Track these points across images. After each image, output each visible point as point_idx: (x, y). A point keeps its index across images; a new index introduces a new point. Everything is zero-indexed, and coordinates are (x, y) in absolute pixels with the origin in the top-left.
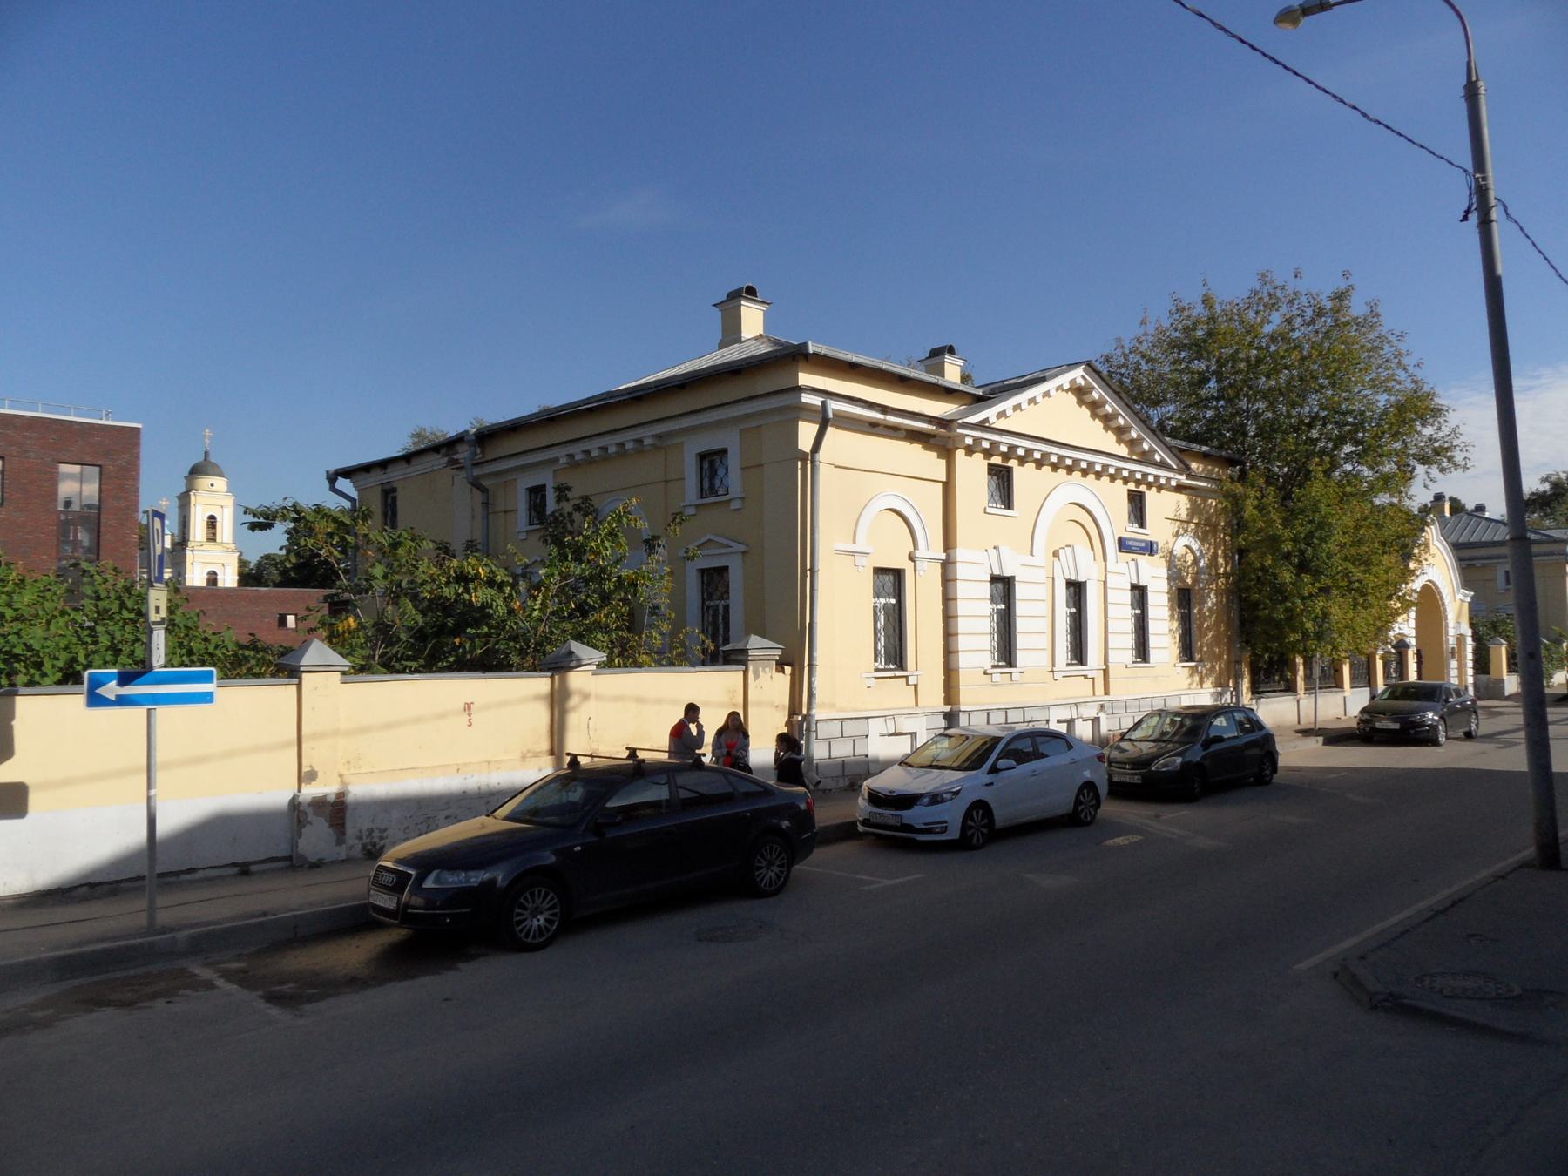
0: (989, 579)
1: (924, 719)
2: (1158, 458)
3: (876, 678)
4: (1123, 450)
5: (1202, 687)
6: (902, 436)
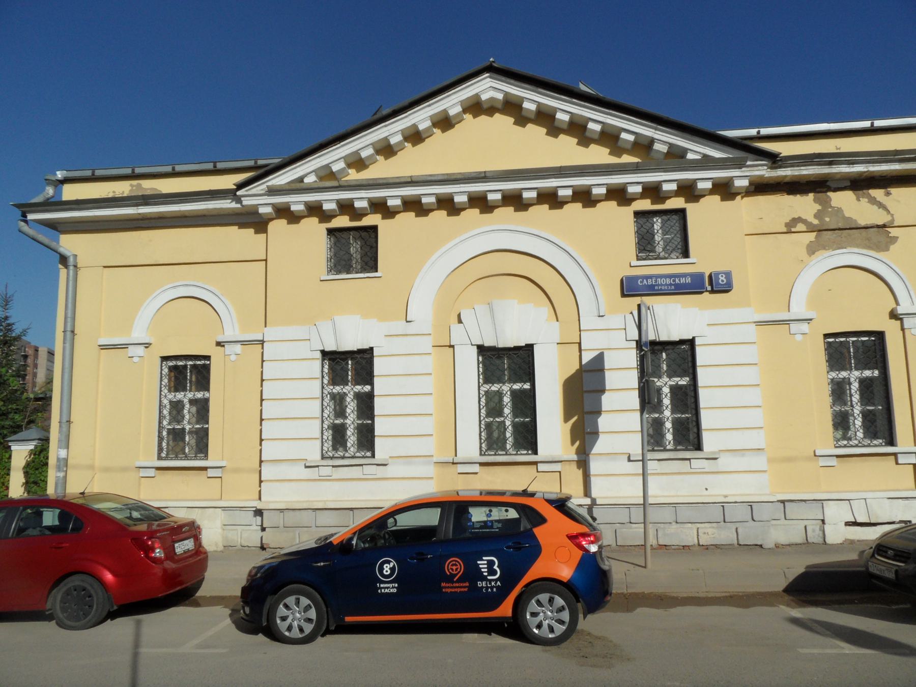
3: (482, 464)
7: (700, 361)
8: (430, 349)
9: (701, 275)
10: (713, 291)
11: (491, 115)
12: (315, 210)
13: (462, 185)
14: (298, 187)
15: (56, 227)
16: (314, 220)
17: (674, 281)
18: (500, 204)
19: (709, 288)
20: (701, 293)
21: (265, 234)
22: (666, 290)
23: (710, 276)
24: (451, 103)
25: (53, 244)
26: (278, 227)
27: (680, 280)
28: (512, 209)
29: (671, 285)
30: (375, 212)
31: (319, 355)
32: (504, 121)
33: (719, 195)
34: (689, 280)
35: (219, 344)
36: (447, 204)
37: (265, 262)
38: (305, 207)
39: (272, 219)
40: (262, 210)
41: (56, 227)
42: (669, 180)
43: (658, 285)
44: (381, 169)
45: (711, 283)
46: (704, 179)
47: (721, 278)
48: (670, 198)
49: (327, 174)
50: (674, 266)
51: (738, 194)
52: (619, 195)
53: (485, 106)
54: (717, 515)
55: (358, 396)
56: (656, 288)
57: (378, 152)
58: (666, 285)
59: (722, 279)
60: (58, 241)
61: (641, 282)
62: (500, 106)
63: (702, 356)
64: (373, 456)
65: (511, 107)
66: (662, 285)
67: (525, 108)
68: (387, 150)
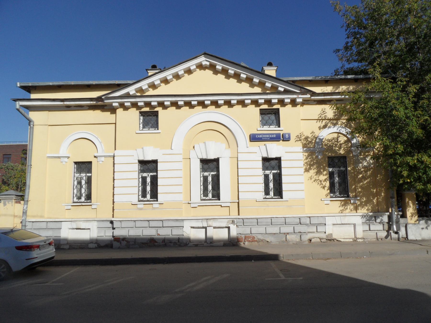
0: (261, 160)
1: (95, 224)
2: (282, 90)
4: (258, 90)
5: (357, 212)
6: (87, 109)
7: (283, 166)
8: (182, 160)
9: (280, 134)
10: (283, 140)
11: (205, 70)
12: (135, 105)
13: (271, 96)
14: (128, 96)
15: (29, 108)
16: (135, 109)
17: (269, 136)
18: (197, 105)
19: (282, 139)
20: (279, 141)
21: (115, 115)
22: (267, 139)
23: (283, 135)
24: (192, 64)
25: (26, 114)
26: (120, 111)
27: (271, 136)
28: (201, 107)
29: (268, 137)
30: (121, 108)
31: (137, 162)
32: (209, 72)
33: (267, 105)
34: (275, 136)
35: (95, 157)
36: (188, 104)
37: (114, 124)
38: (119, 104)
39: (118, 108)
40: (114, 104)
41: (29, 108)
42: (275, 98)
43: (264, 138)
44: (163, 90)
45: (283, 137)
46: (287, 98)
47: (287, 136)
48: (262, 105)
49: (140, 90)
50: (272, 129)
51: (298, 104)
52: (255, 103)
53: (204, 66)
54: (283, 220)
55: (152, 176)
56: (263, 139)
57: (162, 82)
58: (266, 137)
59: (287, 136)
60: (28, 114)
61: (257, 136)
62: (208, 66)
63: (284, 164)
64: (157, 201)
65: (212, 67)
66: (265, 138)
67: (217, 68)
68: (166, 81)
